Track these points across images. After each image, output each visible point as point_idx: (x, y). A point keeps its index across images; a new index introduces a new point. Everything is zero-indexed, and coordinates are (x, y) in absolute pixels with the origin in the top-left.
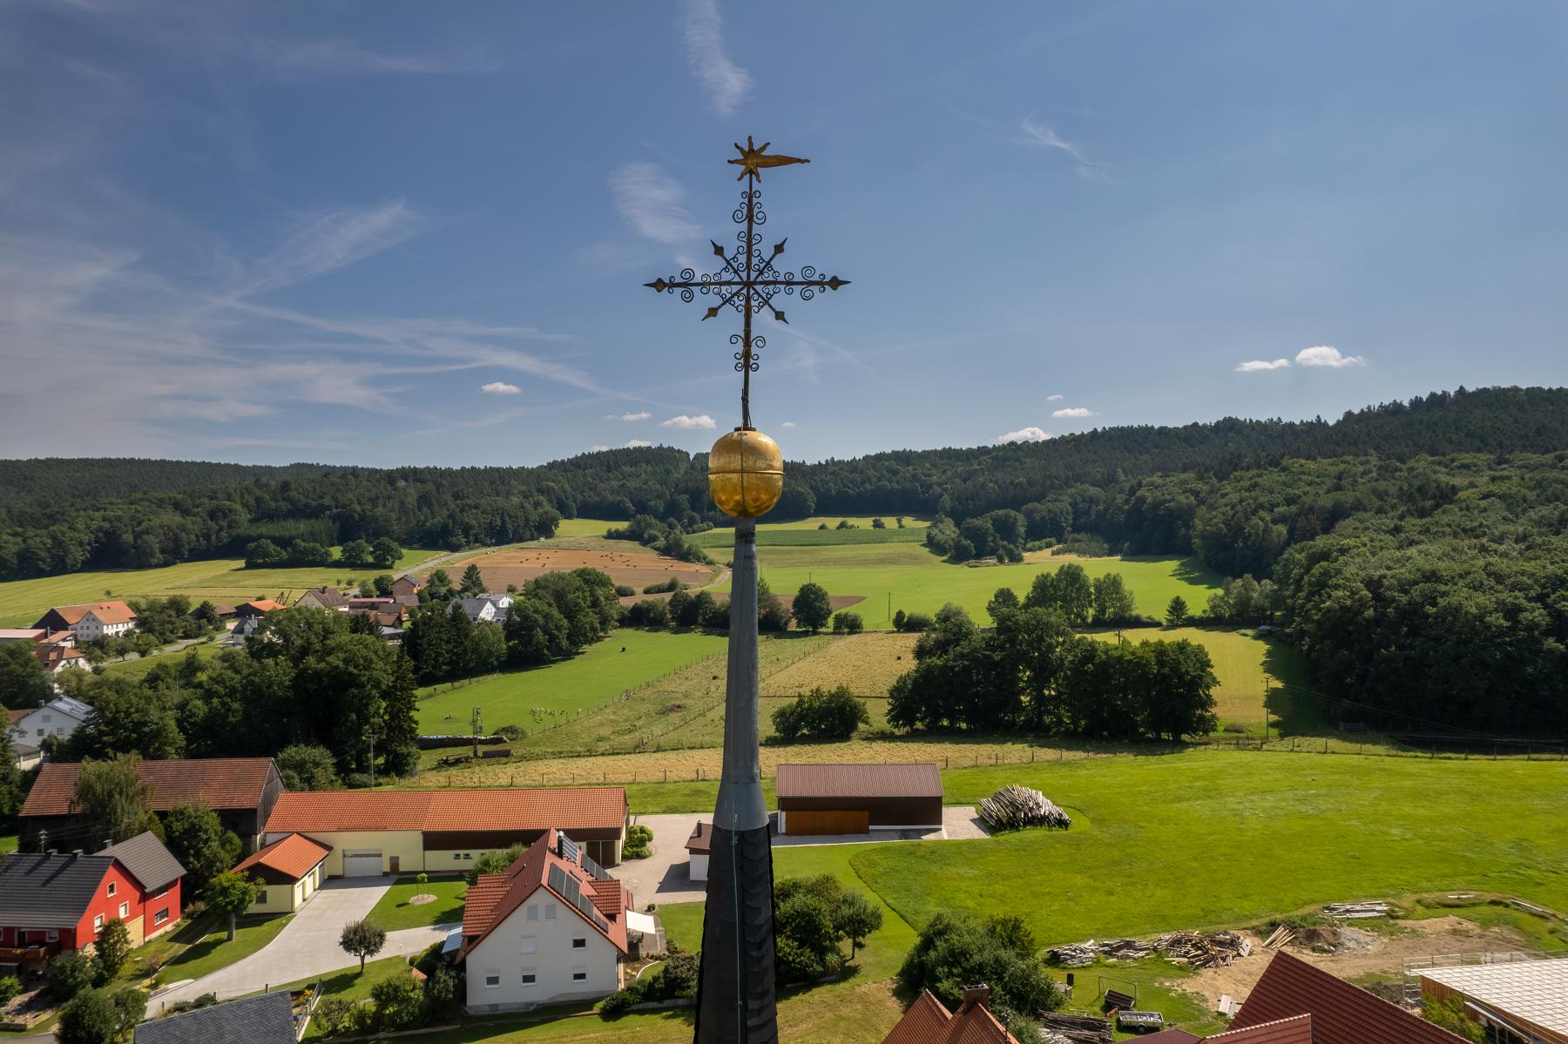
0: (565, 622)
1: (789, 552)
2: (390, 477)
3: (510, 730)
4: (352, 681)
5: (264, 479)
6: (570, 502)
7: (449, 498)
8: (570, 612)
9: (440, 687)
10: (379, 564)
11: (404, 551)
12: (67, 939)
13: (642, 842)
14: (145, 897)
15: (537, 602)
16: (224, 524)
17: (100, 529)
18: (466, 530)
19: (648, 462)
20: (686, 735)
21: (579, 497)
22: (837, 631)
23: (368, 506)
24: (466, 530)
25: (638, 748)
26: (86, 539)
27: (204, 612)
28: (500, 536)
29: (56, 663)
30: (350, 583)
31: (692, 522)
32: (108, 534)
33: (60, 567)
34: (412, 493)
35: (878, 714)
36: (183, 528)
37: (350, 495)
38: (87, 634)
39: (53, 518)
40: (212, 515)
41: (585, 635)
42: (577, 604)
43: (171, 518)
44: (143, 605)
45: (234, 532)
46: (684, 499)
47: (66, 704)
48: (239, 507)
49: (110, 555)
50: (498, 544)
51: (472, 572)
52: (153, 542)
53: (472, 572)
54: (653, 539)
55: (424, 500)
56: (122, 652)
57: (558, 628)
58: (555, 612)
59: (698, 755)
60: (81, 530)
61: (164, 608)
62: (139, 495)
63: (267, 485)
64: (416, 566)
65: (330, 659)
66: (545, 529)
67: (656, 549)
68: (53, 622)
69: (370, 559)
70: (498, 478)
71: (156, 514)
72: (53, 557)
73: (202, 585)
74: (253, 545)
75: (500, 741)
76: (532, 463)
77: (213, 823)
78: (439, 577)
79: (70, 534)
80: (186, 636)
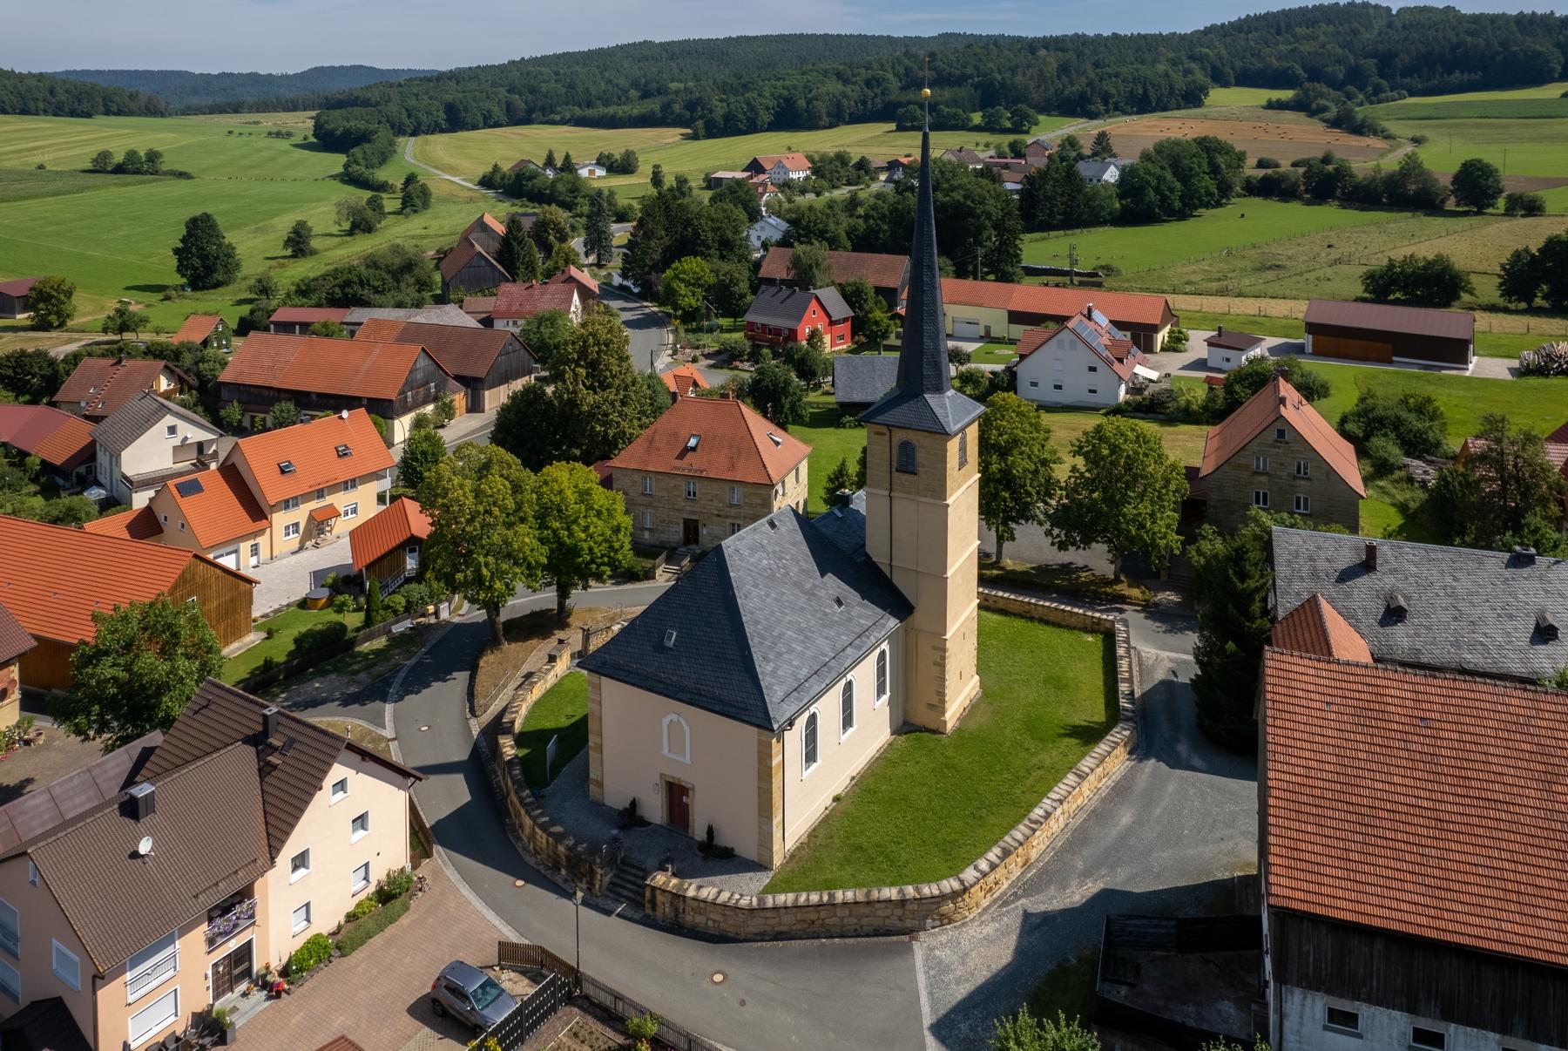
0: (1178, 185)
1: (1505, 127)
2: (1032, 46)
3: (1108, 269)
4: (971, 213)
5: (914, 50)
6: (1228, 70)
7: (1089, 67)
8: (1184, 175)
9: (1053, 233)
10: (1017, 129)
11: (1041, 118)
12: (793, 335)
13: (1179, 340)
14: (832, 323)
15: (1150, 166)
16: (878, 91)
17: (780, 96)
18: (1106, 99)
19: (1329, 22)
20: (1275, 288)
21: (1239, 64)
22: (1510, 212)
23: (1008, 75)
24: (1106, 99)
25: (1222, 293)
26: (771, 104)
27: (862, 165)
28: (1142, 104)
29: (762, 195)
30: (987, 146)
31: (1378, 90)
32: (787, 100)
33: (752, 128)
34: (1051, 61)
35: (1488, 289)
36: (845, 96)
37: (991, 65)
38: (780, 178)
39: (746, 87)
40: (868, 84)
41: (1199, 199)
42: (1191, 169)
43: (834, 86)
44: (816, 158)
45: (887, 99)
46: (1370, 64)
47: (774, 220)
48: (891, 76)
49: (789, 118)
50: (1140, 112)
51: (1102, 138)
52: (821, 107)
53: (1102, 138)
54: (1324, 109)
55: (1064, 69)
56: (803, 192)
57: (1172, 190)
58: (1169, 175)
59: (1292, 303)
60: (765, 100)
61: (831, 161)
62: (810, 66)
63: (916, 56)
64: (1050, 132)
65: (954, 194)
66: (1192, 98)
67: (1325, 121)
68: (755, 167)
69: (1008, 125)
70: (1145, 46)
71: (823, 83)
72: (748, 119)
73: (859, 144)
74: (902, 110)
75: (1096, 275)
76: (1186, 28)
77: (872, 293)
78: (1071, 142)
79: (760, 100)
80: (849, 184)
